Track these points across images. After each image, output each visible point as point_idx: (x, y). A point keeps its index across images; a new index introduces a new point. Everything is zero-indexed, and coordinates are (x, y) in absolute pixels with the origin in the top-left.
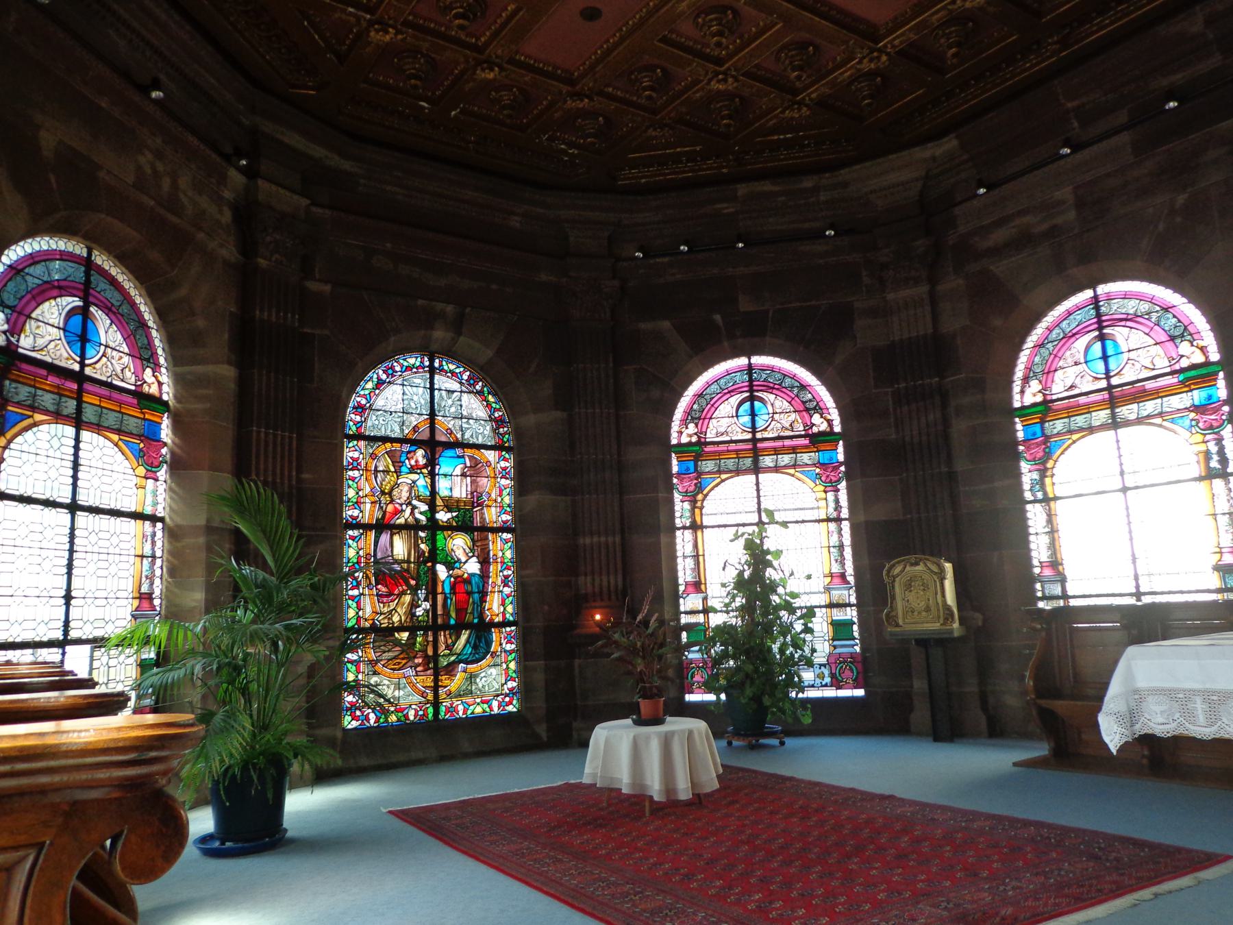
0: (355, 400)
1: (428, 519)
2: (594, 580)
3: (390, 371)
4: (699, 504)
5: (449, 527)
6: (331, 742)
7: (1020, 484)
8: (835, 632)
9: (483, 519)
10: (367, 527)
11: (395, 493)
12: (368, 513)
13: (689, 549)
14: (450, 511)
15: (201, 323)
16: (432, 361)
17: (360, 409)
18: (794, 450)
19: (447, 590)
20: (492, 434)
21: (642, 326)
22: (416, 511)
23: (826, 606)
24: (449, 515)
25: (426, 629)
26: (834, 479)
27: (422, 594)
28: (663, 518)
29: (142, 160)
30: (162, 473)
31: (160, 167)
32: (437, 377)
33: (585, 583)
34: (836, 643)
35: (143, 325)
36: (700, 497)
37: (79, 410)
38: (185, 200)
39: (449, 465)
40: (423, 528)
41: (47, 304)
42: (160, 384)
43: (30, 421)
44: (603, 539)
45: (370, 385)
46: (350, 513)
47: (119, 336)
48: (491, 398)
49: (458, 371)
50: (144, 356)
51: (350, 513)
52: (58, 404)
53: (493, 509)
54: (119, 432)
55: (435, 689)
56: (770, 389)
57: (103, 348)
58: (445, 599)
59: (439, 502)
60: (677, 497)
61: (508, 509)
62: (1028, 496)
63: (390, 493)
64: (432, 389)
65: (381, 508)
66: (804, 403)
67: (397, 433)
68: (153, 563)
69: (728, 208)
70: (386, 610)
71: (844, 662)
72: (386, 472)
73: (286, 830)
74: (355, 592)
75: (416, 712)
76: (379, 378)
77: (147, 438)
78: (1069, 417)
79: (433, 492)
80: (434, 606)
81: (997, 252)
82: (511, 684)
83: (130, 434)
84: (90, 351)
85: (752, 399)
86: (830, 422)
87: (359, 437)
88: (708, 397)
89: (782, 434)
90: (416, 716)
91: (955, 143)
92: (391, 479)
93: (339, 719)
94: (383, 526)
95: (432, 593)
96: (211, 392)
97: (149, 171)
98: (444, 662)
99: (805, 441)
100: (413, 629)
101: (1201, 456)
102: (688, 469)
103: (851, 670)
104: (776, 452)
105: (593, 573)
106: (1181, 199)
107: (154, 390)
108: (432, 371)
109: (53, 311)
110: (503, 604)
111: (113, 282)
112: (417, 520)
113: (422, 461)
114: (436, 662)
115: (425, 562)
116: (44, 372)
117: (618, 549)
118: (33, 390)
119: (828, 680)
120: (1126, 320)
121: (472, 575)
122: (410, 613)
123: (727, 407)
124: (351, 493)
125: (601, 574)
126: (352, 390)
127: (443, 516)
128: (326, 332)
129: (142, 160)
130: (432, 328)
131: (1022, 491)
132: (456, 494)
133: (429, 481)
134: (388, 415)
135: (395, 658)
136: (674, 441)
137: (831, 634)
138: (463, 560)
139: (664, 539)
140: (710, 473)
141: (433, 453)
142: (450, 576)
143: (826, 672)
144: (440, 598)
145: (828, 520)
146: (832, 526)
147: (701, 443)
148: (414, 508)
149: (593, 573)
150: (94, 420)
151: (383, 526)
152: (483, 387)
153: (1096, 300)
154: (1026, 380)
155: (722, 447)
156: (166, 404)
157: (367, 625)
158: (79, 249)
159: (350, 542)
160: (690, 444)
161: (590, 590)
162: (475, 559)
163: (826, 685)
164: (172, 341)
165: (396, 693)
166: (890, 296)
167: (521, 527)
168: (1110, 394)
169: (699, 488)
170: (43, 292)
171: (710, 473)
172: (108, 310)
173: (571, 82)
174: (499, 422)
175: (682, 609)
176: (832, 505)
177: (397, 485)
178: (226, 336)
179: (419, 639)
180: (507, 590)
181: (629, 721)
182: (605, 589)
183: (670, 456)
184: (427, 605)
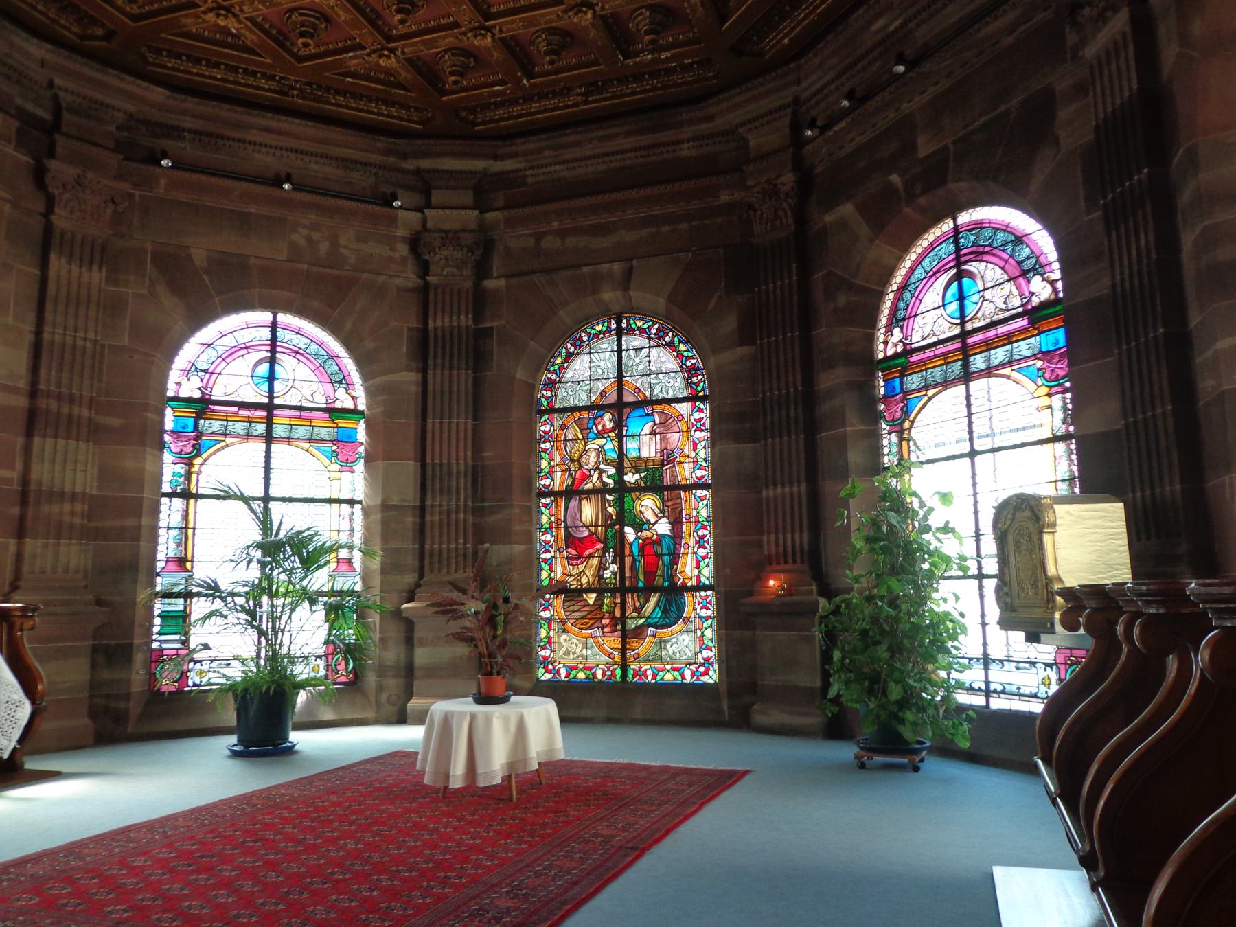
1: (615, 482)
3: (578, 344)
9: (674, 477)
10: (557, 494)
11: (583, 459)
12: (558, 481)
14: (637, 471)
16: (619, 323)
17: (551, 385)
18: (1009, 339)
19: (635, 552)
20: (683, 385)
24: (637, 476)
27: (610, 556)
30: (360, 466)
31: (316, 236)
36: (907, 424)
37: (269, 430)
40: (610, 491)
42: (354, 398)
43: (223, 444)
54: (310, 440)
55: (623, 651)
59: (627, 464)
63: (579, 461)
64: (619, 351)
66: (1019, 263)
67: (585, 401)
70: (575, 572)
72: (576, 440)
74: (548, 555)
87: (551, 410)
90: (604, 674)
94: (573, 492)
95: (620, 556)
98: (632, 625)
99: (1022, 323)
100: (600, 591)
104: (989, 345)
107: (349, 404)
110: (698, 565)
112: (604, 484)
113: (609, 425)
114: (624, 625)
115: (612, 525)
116: (235, 409)
118: (225, 423)
121: (660, 537)
125: (793, 532)
127: (631, 478)
132: (645, 453)
135: (583, 618)
141: (620, 416)
144: (628, 560)
147: (908, 351)
148: (602, 472)
151: (573, 492)
152: (673, 337)
155: (929, 353)
156: (362, 412)
160: (896, 355)
162: (665, 520)
167: (717, 483)
169: (906, 413)
174: (691, 372)
179: (606, 601)
180: (702, 552)
182: (790, 550)
183: (873, 377)
184: (614, 568)
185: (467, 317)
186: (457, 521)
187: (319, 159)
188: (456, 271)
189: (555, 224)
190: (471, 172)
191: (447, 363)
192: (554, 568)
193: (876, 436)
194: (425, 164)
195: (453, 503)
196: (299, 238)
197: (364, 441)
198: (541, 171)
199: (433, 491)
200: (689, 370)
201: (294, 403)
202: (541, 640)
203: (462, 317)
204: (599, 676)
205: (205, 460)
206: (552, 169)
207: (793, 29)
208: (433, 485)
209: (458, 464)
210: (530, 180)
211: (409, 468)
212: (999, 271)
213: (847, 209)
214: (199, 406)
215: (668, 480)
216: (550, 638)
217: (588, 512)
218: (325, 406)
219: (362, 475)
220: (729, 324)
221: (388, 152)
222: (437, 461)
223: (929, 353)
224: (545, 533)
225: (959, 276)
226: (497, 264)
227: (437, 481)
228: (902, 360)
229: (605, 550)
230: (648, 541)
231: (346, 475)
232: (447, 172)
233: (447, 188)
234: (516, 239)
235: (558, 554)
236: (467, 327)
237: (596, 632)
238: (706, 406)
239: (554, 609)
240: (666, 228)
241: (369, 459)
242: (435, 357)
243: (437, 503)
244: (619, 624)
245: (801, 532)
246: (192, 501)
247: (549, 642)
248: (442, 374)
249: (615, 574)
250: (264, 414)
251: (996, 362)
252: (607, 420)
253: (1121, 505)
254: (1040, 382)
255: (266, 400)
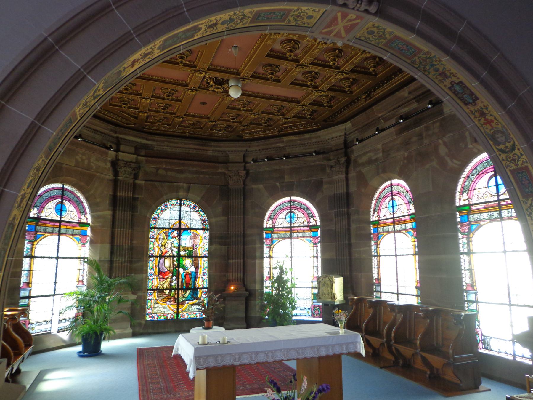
0: (154, 216)
1: (177, 254)
2: (233, 275)
3: (166, 206)
4: (272, 249)
5: (185, 256)
6: (140, 325)
7: (371, 249)
8: (314, 297)
9: (197, 253)
10: (156, 257)
11: (166, 246)
12: (157, 252)
13: (268, 265)
14: (185, 250)
15: (98, 200)
16: (181, 201)
17: (155, 219)
18: (304, 231)
19: (183, 277)
20: (201, 225)
21: (253, 186)
22: (173, 251)
23: (311, 288)
24: (185, 252)
25: (175, 289)
26: (316, 242)
27: (174, 278)
28: (258, 254)
29: (78, 157)
30: (88, 245)
31: (84, 157)
32: (182, 207)
33: (230, 276)
34: (314, 301)
35: (81, 202)
36: (272, 246)
37: (60, 230)
38: (92, 165)
39: (185, 236)
40: (175, 257)
41: (50, 203)
42: (87, 219)
43: (44, 236)
44: (237, 261)
45: (159, 211)
46: (150, 252)
47: (73, 207)
48: (201, 213)
49: (190, 204)
50: (82, 211)
51: (150, 252)
52: (53, 230)
53: (200, 250)
54: (72, 235)
55: (178, 309)
56: (297, 209)
57: (67, 212)
58: (182, 280)
59: (181, 248)
60: (265, 246)
61: (206, 250)
62: (373, 254)
63: (164, 246)
64: (180, 211)
65: (161, 250)
66: (308, 214)
67: (167, 226)
68: (84, 271)
69: (282, 145)
70: (161, 283)
71: (316, 308)
72: (164, 239)
73: (102, 351)
74: (152, 278)
75: (171, 316)
76: (162, 209)
77: (82, 235)
78: (384, 227)
79: (179, 245)
80: (178, 282)
81: (363, 164)
82: (156, 317)
83: (76, 235)
84: (63, 213)
85: (291, 212)
86: (316, 221)
87: (155, 228)
88: (276, 211)
89: (300, 225)
90: (170, 317)
91: (351, 124)
92: (165, 241)
93: (144, 317)
94: (161, 257)
95: (178, 278)
96: (102, 220)
97: (80, 160)
98: (181, 300)
99: (307, 228)
100: (170, 289)
101: (414, 246)
102: (269, 236)
103: (318, 311)
104: (298, 231)
105: (232, 272)
106: (406, 154)
107: (85, 221)
108: (181, 205)
109: (52, 205)
110: (203, 282)
111: (71, 192)
112: (173, 254)
113: (176, 235)
114: (178, 300)
115: (176, 268)
116: (49, 222)
117: (242, 264)
118: (45, 227)
119: (310, 314)
120: (398, 194)
121: (192, 272)
122: (170, 284)
123: (282, 215)
124: (151, 246)
125: (238, 273)
126: (152, 213)
127: (182, 253)
128: (143, 196)
129: (78, 157)
130: (179, 192)
131: (371, 252)
132: (187, 246)
133: (178, 241)
134: (164, 220)
135: (164, 298)
136: (265, 227)
137: (312, 298)
138: (189, 267)
139: (258, 261)
140: (276, 238)
141: (180, 232)
142: (184, 272)
143: (310, 311)
144: (180, 280)
145: (314, 257)
146: (315, 259)
147: (273, 228)
148: (172, 250)
149: (232, 272)
150: (64, 232)
151: (161, 257)
152: (199, 209)
153: (391, 185)
154: (374, 211)
155: (280, 229)
156: (89, 224)
157: (155, 288)
158: (60, 185)
159: (151, 262)
160: (270, 228)
161: (231, 278)
162: (193, 267)
163: (309, 316)
164: (90, 206)
165: (164, 310)
166: (334, 178)
167: (211, 256)
168: (394, 220)
169: (272, 243)
170: (48, 200)
171: (276, 238)
172: (69, 200)
173: (208, 118)
174: (204, 221)
175: (265, 285)
176: (315, 251)
177: (167, 243)
178: (108, 202)
179: (172, 293)
180: (204, 277)
181: (201, 328)
182: (236, 278)
183: (263, 232)
184: (176, 282)
185: (131, 193)
186: (124, 266)
187: (86, 128)
188: (128, 176)
189: (164, 166)
190: (136, 142)
191: (123, 209)
192: (154, 281)
193: (262, 248)
194: (121, 136)
195: (123, 260)
196: (78, 158)
197: (90, 235)
198: (160, 147)
199: (117, 255)
200: (203, 220)
201: (68, 220)
202: (148, 307)
203: (129, 193)
204: (169, 317)
205: (38, 243)
206: (164, 147)
207: (254, 136)
208: (117, 252)
209: (125, 245)
210: (155, 149)
211: (107, 246)
212: (302, 214)
213: (261, 186)
214: (36, 221)
215: (194, 255)
216: (151, 306)
217: (167, 263)
218: (77, 221)
219: (88, 248)
220: (220, 209)
221: (111, 130)
222: (118, 244)
223: (280, 229)
224: (151, 269)
225: (291, 212)
226: (141, 176)
227: (118, 251)
228: (272, 229)
229: (173, 276)
230: (187, 274)
231: (83, 248)
232: (128, 140)
233: (126, 145)
234: (149, 168)
235: (155, 277)
236: (130, 197)
237: (168, 303)
238: (208, 232)
239: (154, 296)
240: (202, 176)
241: (92, 242)
242: (119, 207)
243: (118, 259)
244: (177, 300)
245: (240, 273)
246: (33, 259)
247: (151, 307)
248: (122, 213)
249: (176, 284)
250: (58, 224)
251: (300, 236)
252: (175, 233)
253: (342, 278)
254: (311, 243)
255: (59, 219)
